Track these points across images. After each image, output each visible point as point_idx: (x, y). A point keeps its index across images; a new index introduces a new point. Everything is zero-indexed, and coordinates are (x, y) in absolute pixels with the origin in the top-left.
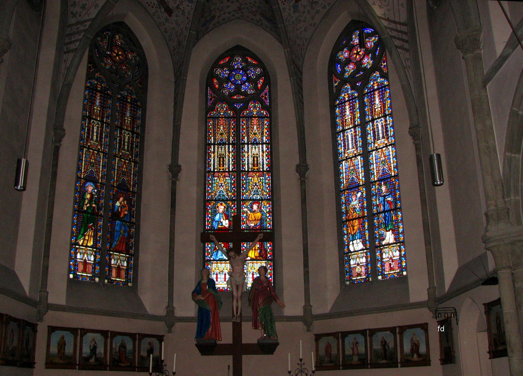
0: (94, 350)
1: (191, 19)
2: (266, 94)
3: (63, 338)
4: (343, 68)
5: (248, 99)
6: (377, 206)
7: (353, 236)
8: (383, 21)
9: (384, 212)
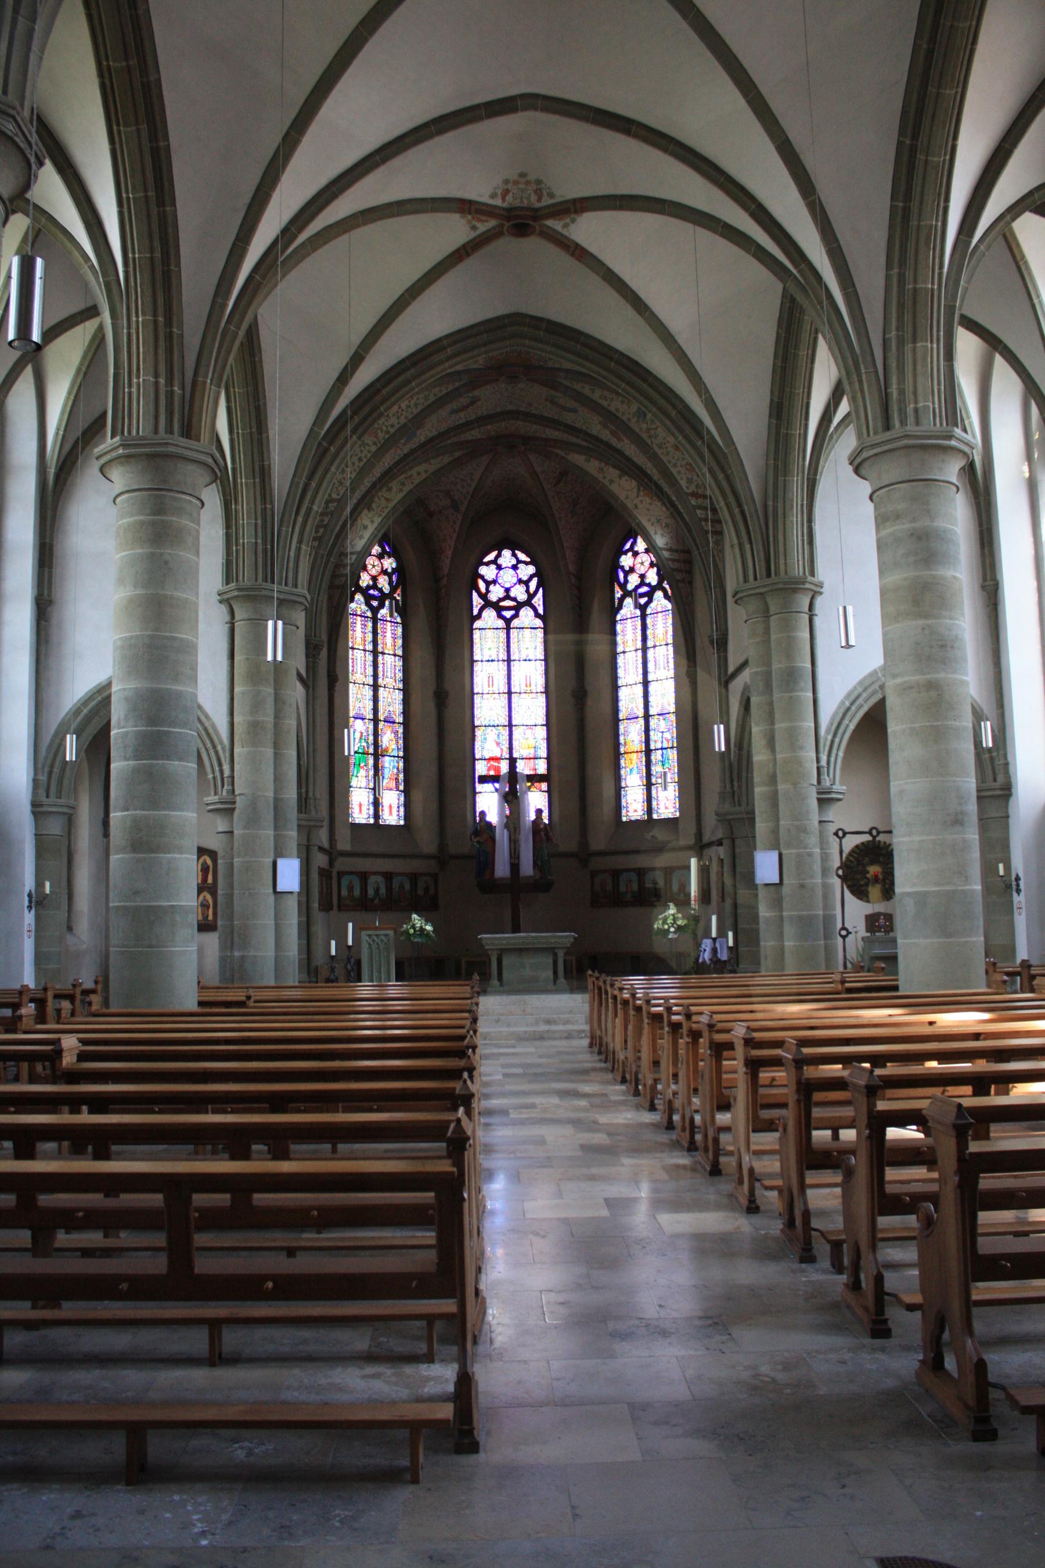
0: (377, 890)
1: (457, 530)
2: (539, 600)
3: (351, 882)
4: (626, 577)
5: (518, 607)
6: (656, 741)
7: (631, 770)
8: (664, 552)
9: (662, 749)
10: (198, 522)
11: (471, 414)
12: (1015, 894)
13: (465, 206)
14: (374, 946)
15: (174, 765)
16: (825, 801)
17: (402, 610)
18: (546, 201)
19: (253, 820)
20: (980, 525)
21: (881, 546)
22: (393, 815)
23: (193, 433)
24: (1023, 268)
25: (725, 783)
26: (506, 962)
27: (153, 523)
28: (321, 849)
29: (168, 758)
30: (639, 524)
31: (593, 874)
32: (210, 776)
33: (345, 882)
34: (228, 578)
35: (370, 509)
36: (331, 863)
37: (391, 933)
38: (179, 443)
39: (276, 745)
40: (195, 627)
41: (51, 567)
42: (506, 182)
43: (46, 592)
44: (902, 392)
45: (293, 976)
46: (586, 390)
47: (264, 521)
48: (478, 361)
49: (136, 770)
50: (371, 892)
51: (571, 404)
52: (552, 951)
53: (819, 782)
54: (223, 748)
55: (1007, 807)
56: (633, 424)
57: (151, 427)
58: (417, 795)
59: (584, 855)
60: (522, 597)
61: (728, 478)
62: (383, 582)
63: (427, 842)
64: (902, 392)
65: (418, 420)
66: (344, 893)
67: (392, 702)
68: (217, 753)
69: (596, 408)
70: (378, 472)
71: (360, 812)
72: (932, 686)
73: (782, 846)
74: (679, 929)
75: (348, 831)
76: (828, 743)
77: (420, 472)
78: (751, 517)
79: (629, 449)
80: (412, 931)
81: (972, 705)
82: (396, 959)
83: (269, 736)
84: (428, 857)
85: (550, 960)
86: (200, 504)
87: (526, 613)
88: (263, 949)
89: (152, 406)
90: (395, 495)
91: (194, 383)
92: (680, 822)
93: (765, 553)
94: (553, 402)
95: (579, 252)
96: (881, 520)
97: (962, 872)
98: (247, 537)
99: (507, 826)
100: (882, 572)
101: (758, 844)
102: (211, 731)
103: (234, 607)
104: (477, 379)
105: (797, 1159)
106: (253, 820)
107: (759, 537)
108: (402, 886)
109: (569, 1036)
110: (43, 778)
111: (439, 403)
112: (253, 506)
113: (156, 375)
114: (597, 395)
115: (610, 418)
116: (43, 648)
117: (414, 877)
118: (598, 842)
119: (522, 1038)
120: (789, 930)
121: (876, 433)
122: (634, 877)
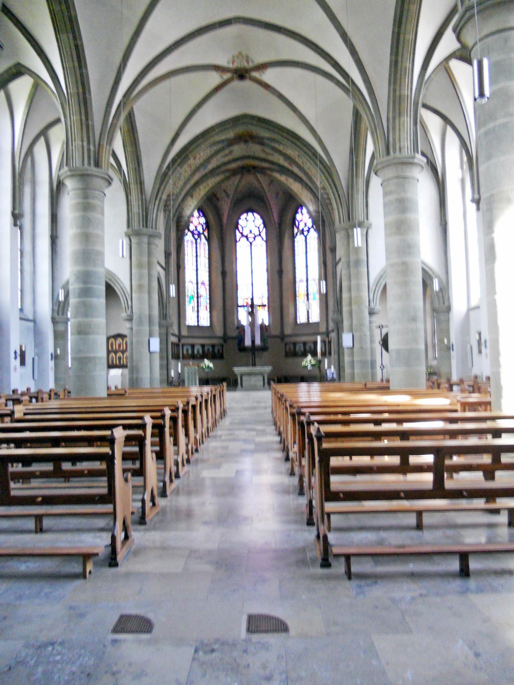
10: (103, 202)
11: (230, 157)
12: (451, 351)
13: (217, 68)
14: (190, 373)
15: (95, 300)
16: (371, 313)
17: (208, 239)
18: (251, 65)
19: (140, 322)
20: (440, 197)
21: (385, 205)
22: (205, 322)
23: (100, 165)
24: (455, 85)
25: (335, 306)
26: (244, 378)
27: (83, 203)
28: (173, 335)
29: (92, 297)
30: (303, 203)
31: (286, 345)
32: (124, 307)
33: (185, 348)
34: (128, 226)
35: (192, 197)
36: (179, 341)
37: (197, 368)
38: (93, 170)
39: (149, 293)
40: (103, 245)
41: (56, 222)
42: (233, 57)
43: (54, 233)
44: (394, 140)
45: (157, 384)
46: (277, 146)
47: (142, 203)
48: (231, 134)
49: (79, 303)
50: (196, 352)
51: (271, 152)
52: (262, 374)
53: (369, 305)
54: (128, 295)
55: (449, 315)
56: (297, 159)
57: (81, 163)
58: (215, 313)
59: (282, 337)
60: (257, 233)
61: (333, 181)
62: (200, 229)
63: (219, 331)
64: (394, 140)
65: (208, 160)
66: (185, 352)
67: (204, 276)
68: (126, 297)
69: (280, 153)
70: (192, 182)
71: (191, 320)
72: (404, 264)
73: (354, 330)
74: (312, 365)
75: (186, 328)
76: (373, 290)
77: (212, 182)
78: (342, 196)
79: (296, 170)
80: (204, 367)
81: (423, 269)
82: (199, 378)
83: (146, 289)
84: (219, 338)
85: (261, 378)
86: (104, 195)
87: (258, 239)
88: (145, 375)
89: (81, 154)
90: (202, 191)
91: (99, 145)
92: (320, 324)
93: (348, 211)
94: (264, 151)
95: (267, 86)
96: (385, 194)
97: (415, 340)
98: (136, 209)
99: (250, 325)
100: (385, 216)
101: (345, 330)
102: (124, 289)
103: (131, 238)
104: (231, 143)
105: (94, 418)
106: (140, 322)
107: (345, 204)
108: (208, 350)
109: (266, 408)
110: (56, 308)
111: (217, 152)
112: (137, 197)
113: (82, 141)
114: (281, 148)
115: (287, 157)
116: (54, 256)
117: (213, 346)
118: (288, 331)
119: (246, 409)
120: (356, 366)
121: (383, 157)
122: (302, 345)
